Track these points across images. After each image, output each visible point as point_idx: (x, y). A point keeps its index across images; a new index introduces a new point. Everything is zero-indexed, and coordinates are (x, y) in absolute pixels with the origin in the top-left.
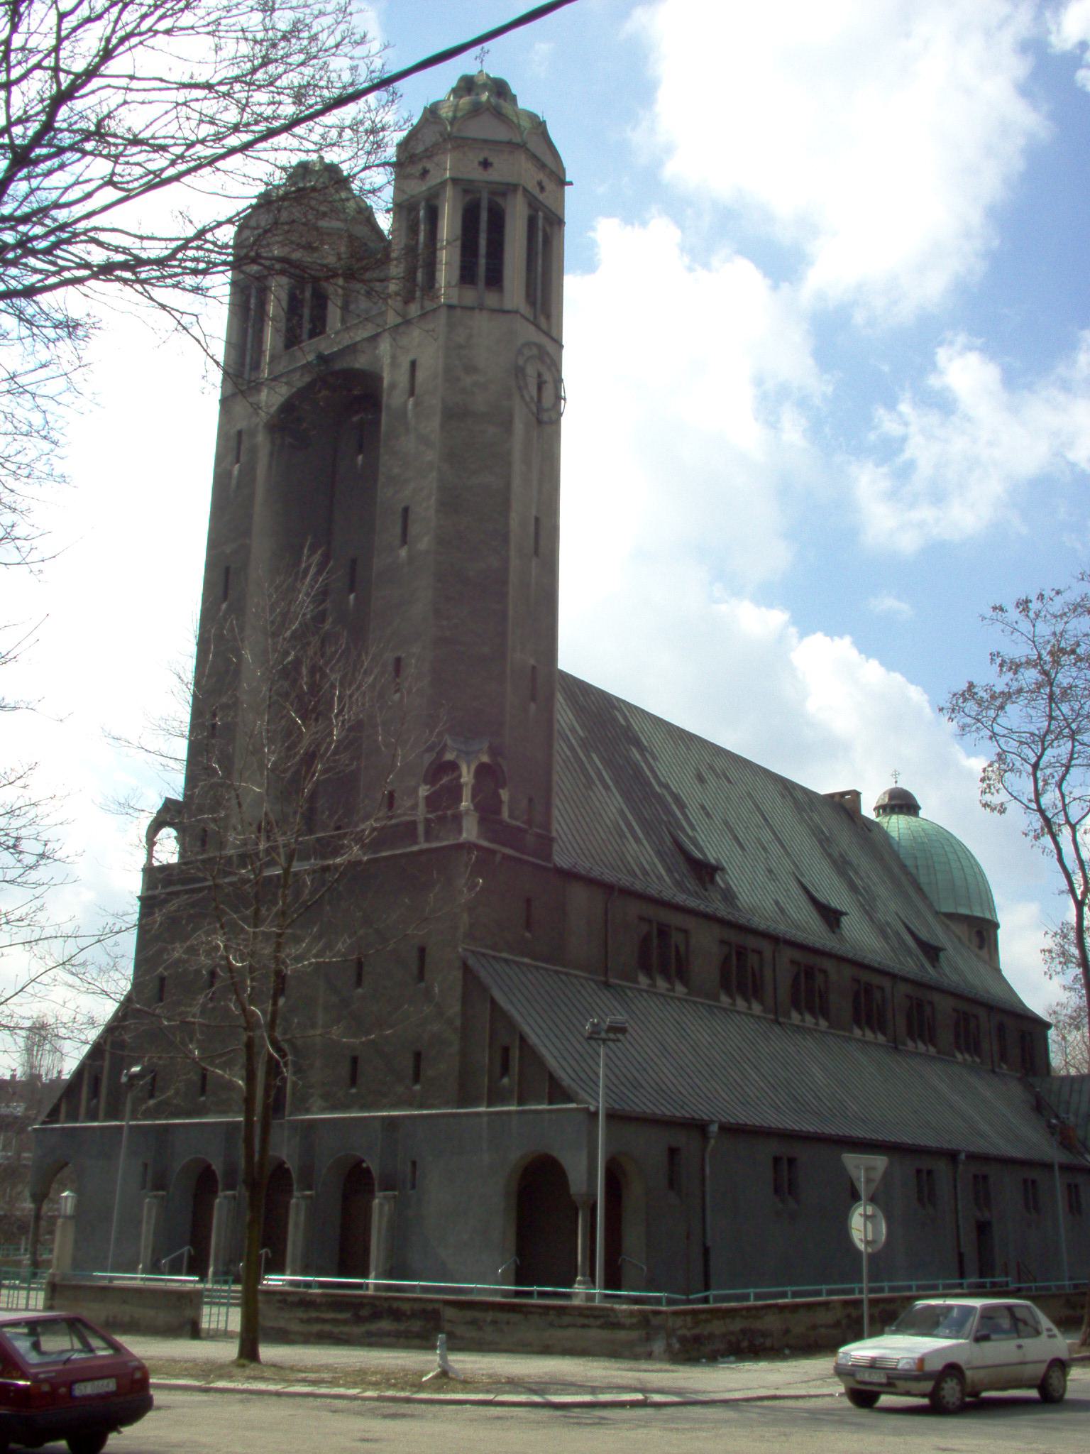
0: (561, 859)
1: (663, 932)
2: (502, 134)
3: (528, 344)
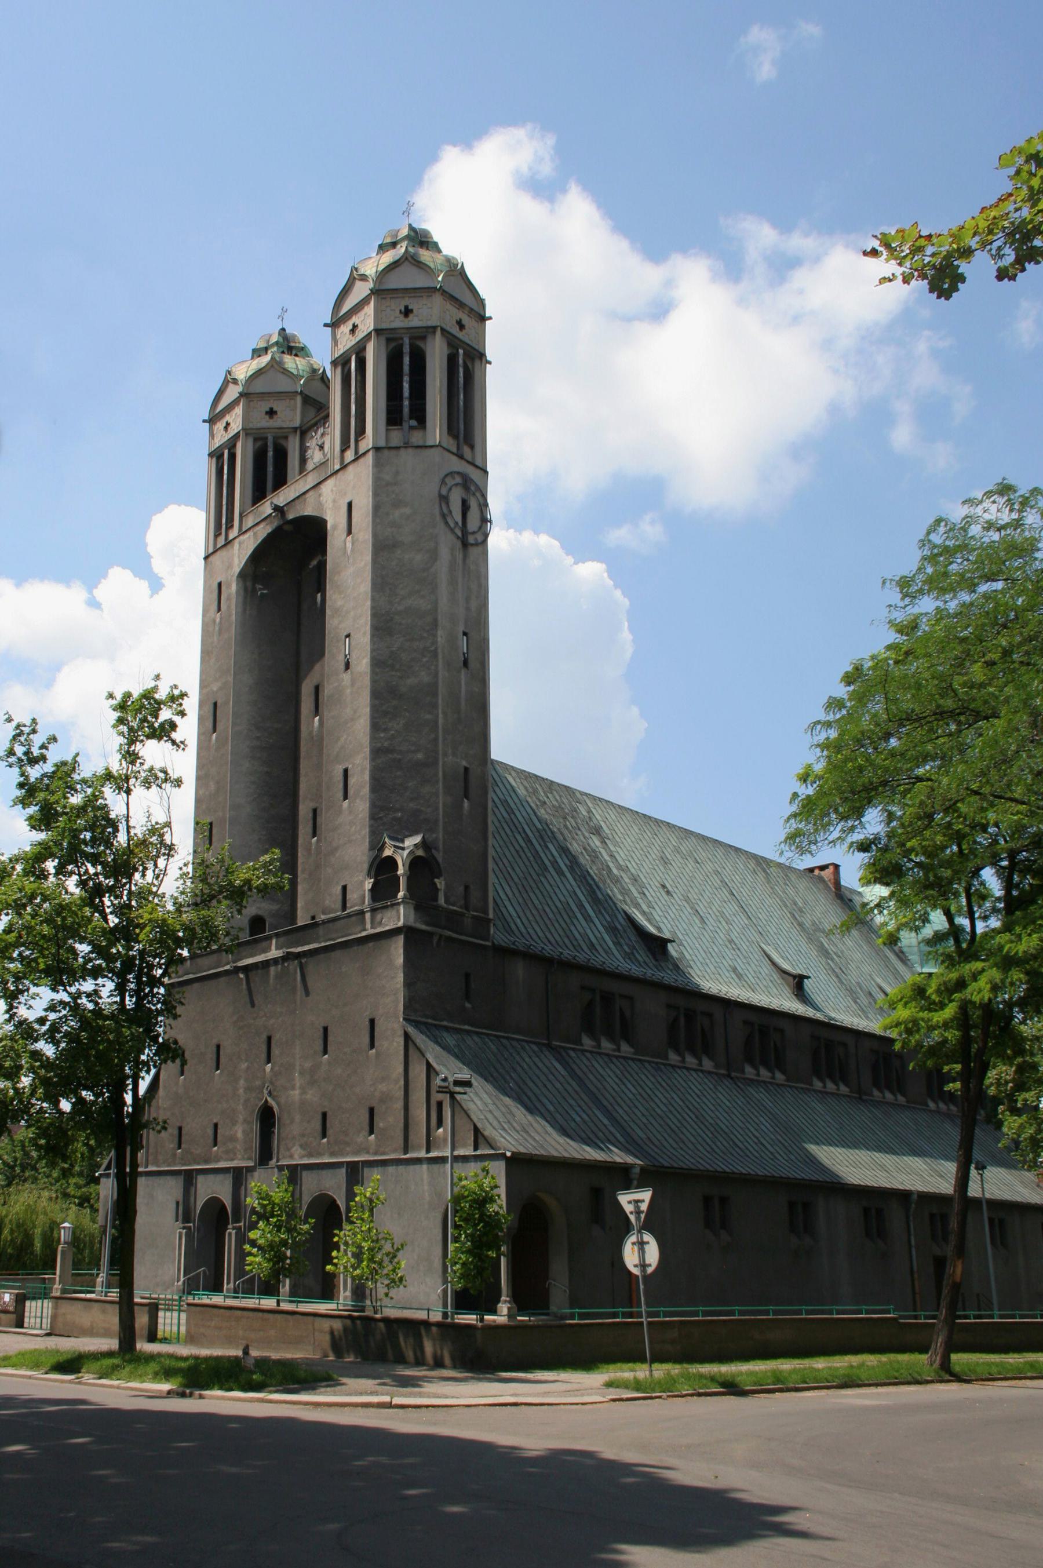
0: (498, 936)
1: (607, 998)
2: (420, 281)
3: (451, 474)
